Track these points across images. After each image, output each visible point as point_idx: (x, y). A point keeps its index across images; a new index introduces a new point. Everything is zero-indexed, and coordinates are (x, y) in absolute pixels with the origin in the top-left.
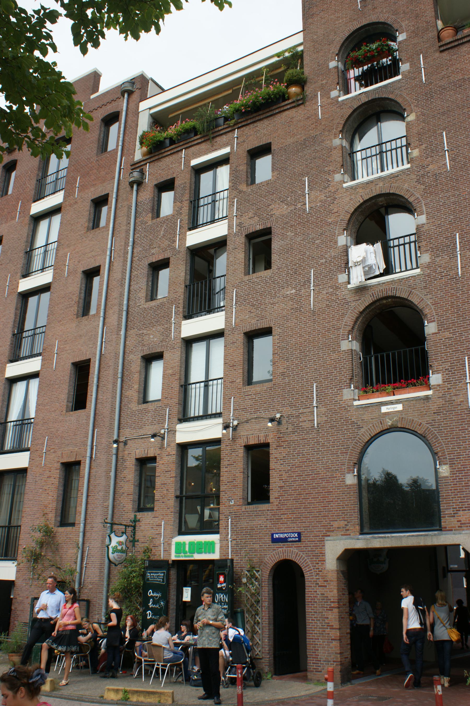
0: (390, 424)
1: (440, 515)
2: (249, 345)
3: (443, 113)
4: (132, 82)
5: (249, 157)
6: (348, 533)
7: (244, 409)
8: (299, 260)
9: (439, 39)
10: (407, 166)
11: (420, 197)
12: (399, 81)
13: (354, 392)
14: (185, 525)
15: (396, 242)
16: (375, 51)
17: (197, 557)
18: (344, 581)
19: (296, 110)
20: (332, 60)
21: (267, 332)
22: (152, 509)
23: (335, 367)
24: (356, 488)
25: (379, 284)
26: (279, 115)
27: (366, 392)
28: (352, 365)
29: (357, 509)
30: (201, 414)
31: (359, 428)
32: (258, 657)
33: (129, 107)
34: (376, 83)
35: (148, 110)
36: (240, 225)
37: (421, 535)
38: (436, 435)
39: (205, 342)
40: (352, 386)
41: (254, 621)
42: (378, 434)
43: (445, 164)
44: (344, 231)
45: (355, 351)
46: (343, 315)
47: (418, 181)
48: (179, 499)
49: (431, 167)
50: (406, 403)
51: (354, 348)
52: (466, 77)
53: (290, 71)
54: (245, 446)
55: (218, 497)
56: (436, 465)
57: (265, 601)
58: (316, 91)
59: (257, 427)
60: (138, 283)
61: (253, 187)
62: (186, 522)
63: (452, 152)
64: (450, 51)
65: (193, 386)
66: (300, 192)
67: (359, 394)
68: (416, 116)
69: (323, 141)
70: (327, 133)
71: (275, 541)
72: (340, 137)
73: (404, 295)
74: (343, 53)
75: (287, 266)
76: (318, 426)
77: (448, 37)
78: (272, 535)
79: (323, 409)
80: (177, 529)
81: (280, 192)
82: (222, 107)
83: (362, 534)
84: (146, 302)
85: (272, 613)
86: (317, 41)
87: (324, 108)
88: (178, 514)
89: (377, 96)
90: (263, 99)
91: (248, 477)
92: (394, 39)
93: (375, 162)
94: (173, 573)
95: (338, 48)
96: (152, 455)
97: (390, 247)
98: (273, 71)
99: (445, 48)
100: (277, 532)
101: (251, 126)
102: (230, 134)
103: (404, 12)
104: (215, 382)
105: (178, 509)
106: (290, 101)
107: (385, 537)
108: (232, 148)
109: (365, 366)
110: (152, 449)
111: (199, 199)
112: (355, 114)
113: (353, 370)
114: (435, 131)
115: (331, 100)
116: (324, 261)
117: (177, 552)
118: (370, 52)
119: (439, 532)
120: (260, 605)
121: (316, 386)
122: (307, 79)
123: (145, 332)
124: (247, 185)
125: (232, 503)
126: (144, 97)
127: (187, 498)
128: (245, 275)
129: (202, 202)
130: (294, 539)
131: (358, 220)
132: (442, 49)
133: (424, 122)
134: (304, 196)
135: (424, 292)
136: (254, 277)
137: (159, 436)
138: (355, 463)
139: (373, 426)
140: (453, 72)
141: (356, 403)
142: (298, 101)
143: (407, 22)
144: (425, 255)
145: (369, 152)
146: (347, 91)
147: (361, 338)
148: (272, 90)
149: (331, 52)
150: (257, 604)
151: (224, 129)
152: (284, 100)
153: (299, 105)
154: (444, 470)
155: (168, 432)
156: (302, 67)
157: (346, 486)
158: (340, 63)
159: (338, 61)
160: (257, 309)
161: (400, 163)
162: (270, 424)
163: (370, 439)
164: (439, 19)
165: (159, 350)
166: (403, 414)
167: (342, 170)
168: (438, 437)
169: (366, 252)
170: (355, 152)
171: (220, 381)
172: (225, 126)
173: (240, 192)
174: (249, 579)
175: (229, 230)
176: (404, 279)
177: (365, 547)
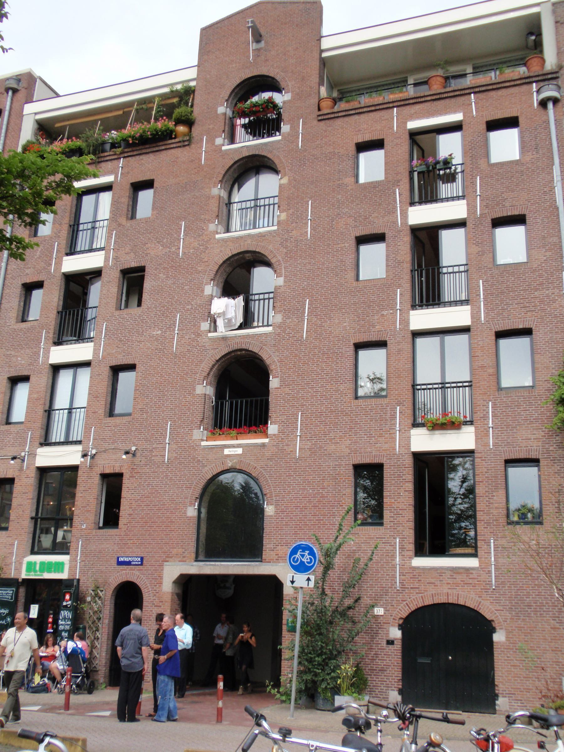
0: (230, 465)
2: (113, 378)
4: (18, 78)
5: (132, 190)
6: (184, 559)
7: (104, 440)
8: (168, 302)
9: (319, 110)
10: (275, 228)
11: (281, 260)
14: (38, 545)
15: (257, 297)
17: (47, 576)
18: (178, 602)
21: (131, 367)
22: (6, 529)
25: (236, 337)
26: (165, 152)
28: (204, 408)
30: (62, 440)
31: (204, 466)
32: (95, 669)
33: (13, 106)
35: (34, 115)
36: (116, 259)
37: (245, 565)
39: (72, 370)
40: (202, 427)
41: (95, 637)
43: (307, 232)
45: (208, 395)
46: (201, 361)
48: (33, 520)
49: (294, 232)
50: (246, 448)
51: (208, 393)
52: (336, 151)
54: (101, 475)
55: (71, 520)
57: (106, 619)
58: (202, 135)
59: (114, 457)
60: (9, 302)
61: (133, 222)
62: (39, 541)
65: (57, 412)
66: (175, 236)
67: (207, 435)
68: (289, 180)
71: (120, 563)
72: (219, 187)
74: (233, 99)
75: (156, 307)
76: (168, 461)
78: (118, 558)
79: (174, 446)
80: (30, 549)
81: (158, 232)
82: (109, 131)
84: (17, 322)
85: (111, 630)
88: (31, 535)
89: (257, 153)
90: (151, 134)
91: (101, 503)
94: (22, 591)
95: (229, 93)
96: (11, 476)
98: (166, 99)
100: (123, 555)
101: (137, 157)
102: (115, 162)
104: (78, 410)
105: (32, 529)
106: (177, 140)
107: (215, 565)
108: (116, 177)
109: (218, 410)
110: (11, 470)
111: (78, 225)
112: (236, 166)
113: (204, 413)
116: (190, 307)
117: (28, 570)
120: (101, 622)
121: (171, 424)
122: (195, 120)
123: (13, 353)
124: (127, 218)
125: (84, 527)
126: (30, 100)
127: (42, 519)
128: (117, 309)
129: (81, 227)
130: (137, 563)
131: (225, 272)
132: (320, 118)
134: (179, 240)
136: (125, 312)
137: (19, 458)
141: (204, 443)
142: (184, 141)
143: (293, 83)
144: (278, 315)
146: (232, 140)
147: (215, 383)
149: (221, 96)
150: (99, 621)
151: (109, 155)
152: (171, 138)
153: (184, 146)
155: (28, 455)
156: (192, 106)
158: (228, 109)
160: (124, 345)
162: (124, 457)
164: (323, 85)
165: (25, 373)
168: (268, 481)
171: (83, 410)
172: (111, 153)
173: (120, 225)
174: (93, 598)
175: (105, 262)
176: (257, 334)
177: (198, 573)
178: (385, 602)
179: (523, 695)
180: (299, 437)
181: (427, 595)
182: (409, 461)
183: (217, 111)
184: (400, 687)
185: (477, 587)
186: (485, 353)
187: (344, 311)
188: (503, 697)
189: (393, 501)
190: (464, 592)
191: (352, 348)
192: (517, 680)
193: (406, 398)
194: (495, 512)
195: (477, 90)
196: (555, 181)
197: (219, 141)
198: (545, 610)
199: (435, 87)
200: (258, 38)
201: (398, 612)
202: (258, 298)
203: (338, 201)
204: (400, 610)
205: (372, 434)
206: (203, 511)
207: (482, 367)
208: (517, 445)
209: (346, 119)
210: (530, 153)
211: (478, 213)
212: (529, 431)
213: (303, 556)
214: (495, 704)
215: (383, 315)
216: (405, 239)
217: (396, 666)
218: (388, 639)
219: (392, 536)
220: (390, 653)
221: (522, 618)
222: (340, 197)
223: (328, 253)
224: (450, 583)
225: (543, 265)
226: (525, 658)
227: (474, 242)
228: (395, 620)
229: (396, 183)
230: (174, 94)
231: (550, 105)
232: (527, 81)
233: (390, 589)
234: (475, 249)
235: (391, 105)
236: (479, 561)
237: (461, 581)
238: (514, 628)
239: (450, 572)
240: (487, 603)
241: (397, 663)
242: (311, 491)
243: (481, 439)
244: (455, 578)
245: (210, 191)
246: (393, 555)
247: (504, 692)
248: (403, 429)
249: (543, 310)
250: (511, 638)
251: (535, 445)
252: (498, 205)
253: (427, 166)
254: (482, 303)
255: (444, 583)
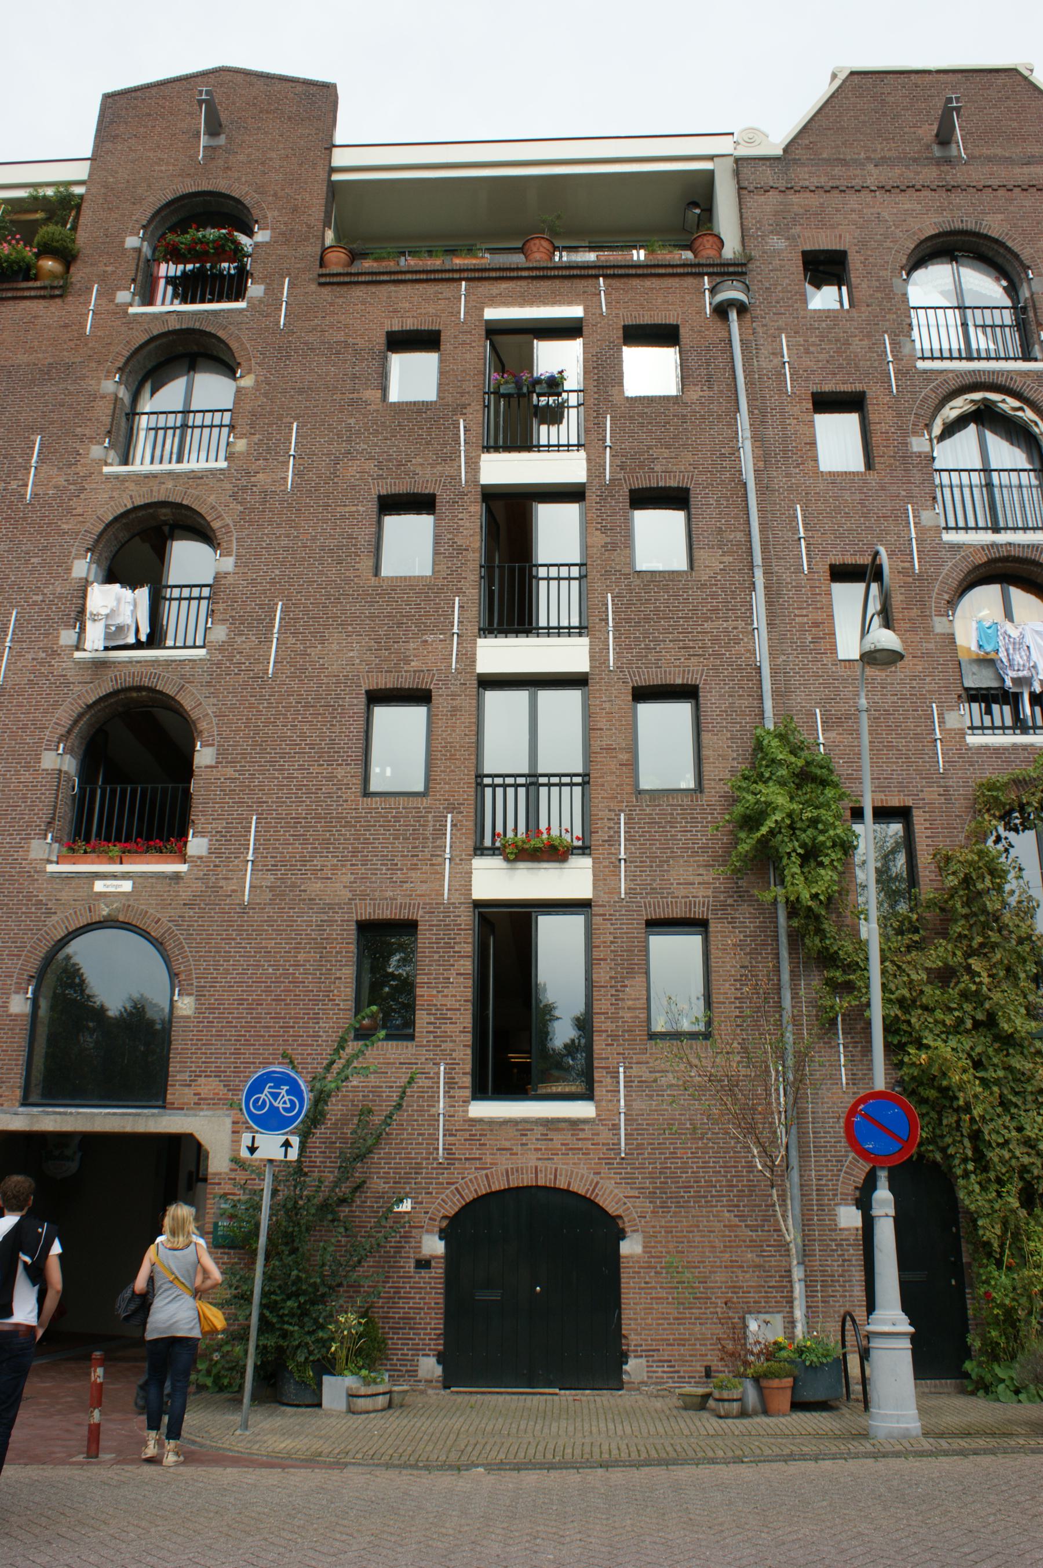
0: (105, 913)
1: (167, 1081)
3: (301, 391)
9: (322, 263)
10: (223, 464)
12: (240, 311)
13: (50, 848)
15: (176, 593)
16: (211, 245)
19: (46, 305)
20: (132, 234)
23: (24, 798)
24: (26, 1023)
25: (131, 662)
26: (11, 303)
27: (73, 851)
28: (57, 798)
29: (22, 1060)
31: (50, 913)
34: (202, 301)
37: (130, 1114)
38: (181, 943)
40: (50, 836)
42: (81, 928)
43: (285, 479)
44: (87, 552)
45: (66, 773)
46: (56, 705)
47: (234, 496)
49: (260, 476)
50: (140, 880)
51: (65, 768)
52: (350, 340)
53: (51, 228)
56: (172, 994)
63: (301, 461)
64: (334, 287)
66: (20, 460)
67: (59, 851)
68: (256, 381)
69: (83, 378)
70: (94, 365)
72: (117, 379)
73: (170, 690)
74: (156, 228)
77: (336, 264)
83: (25, 1104)
86: (113, 189)
87: (98, 317)
89: (197, 326)
92: (250, 233)
93: (171, 442)
95: (149, 215)
97: (166, 599)
98: (19, 212)
99: (328, 280)
103: (275, 195)
106: (38, 284)
107: (65, 1114)
109: (82, 806)
112: (152, 346)
113: (55, 807)
114: (280, 418)
115: (114, 307)
116: (40, 598)
118: (202, 243)
119: (161, 1110)
122: (78, 252)
131: (116, 538)
132: (323, 280)
133: (266, 396)
135: (205, 691)
138: (32, 977)
139: (75, 912)
140: (331, 326)
141: (51, 868)
142: (53, 288)
145: (162, 421)
146: (148, 299)
147: (81, 752)
148: (6, 252)
149: (134, 218)
152: (27, 278)
153: (53, 297)
154: (186, 1005)
156: (74, 228)
157: (8, 1016)
158: (145, 243)
159: (143, 239)
161: (212, 455)
163: (66, 936)
166: (132, 898)
167: (107, 440)
168: (183, 947)
169: (119, 600)
170: (138, 414)
176: (175, 661)
177: (27, 1129)
178: (413, 1186)
179: (672, 1350)
180: (250, 863)
181: (497, 1171)
182: (466, 918)
183: (123, 242)
184: (441, 1347)
185: (591, 1156)
186: (614, 725)
187: (350, 628)
188: (636, 1357)
189: (435, 993)
190: (567, 1164)
191: (363, 699)
192: (662, 1324)
193: (464, 800)
194: (627, 1015)
195: (610, 272)
196: (740, 440)
197: (123, 296)
198: (714, 1193)
199: (537, 256)
200: (214, 128)
201: (439, 1204)
202: (187, 595)
203: (349, 428)
204: (443, 1200)
205: (396, 865)
206: (43, 1004)
207: (609, 749)
208: (668, 893)
209: (373, 289)
210: (698, 388)
211: (608, 477)
212: (691, 869)
213: (275, 1096)
214: (620, 1371)
215: (426, 641)
216: (472, 509)
217: (434, 1308)
218: (418, 1256)
219: (431, 1059)
220: (422, 1285)
221: (673, 1209)
222: (352, 421)
223: (325, 521)
224: (540, 1149)
225: (719, 577)
226: (678, 1283)
227: (599, 526)
228: (435, 1220)
229: (461, 409)
230: (36, 202)
231: (733, 315)
232: (694, 271)
233: (424, 1162)
234: (599, 539)
235: (456, 276)
236: (596, 1107)
237: (562, 1144)
238: (658, 1229)
239: (541, 1128)
240: (610, 1184)
241: (436, 1303)
242: (271, 971)
243: (605, 880)
244: (552, 1140)
245: (99, 384)
246: (433, 1097)
247: (639, 1349)
248: (457, 856)
249: (718, 655)
250: (654, 1247)
251: (700, 894)
252: (641, 466)
253: (518, 385)
254: (611, 633)
255: (530, 1149)
